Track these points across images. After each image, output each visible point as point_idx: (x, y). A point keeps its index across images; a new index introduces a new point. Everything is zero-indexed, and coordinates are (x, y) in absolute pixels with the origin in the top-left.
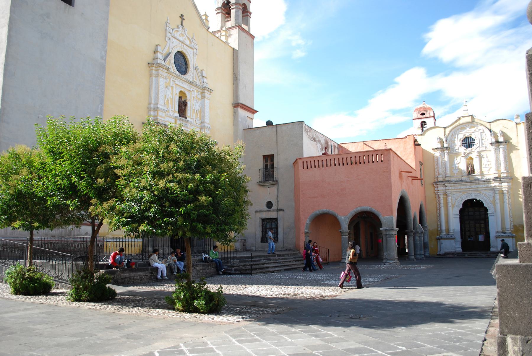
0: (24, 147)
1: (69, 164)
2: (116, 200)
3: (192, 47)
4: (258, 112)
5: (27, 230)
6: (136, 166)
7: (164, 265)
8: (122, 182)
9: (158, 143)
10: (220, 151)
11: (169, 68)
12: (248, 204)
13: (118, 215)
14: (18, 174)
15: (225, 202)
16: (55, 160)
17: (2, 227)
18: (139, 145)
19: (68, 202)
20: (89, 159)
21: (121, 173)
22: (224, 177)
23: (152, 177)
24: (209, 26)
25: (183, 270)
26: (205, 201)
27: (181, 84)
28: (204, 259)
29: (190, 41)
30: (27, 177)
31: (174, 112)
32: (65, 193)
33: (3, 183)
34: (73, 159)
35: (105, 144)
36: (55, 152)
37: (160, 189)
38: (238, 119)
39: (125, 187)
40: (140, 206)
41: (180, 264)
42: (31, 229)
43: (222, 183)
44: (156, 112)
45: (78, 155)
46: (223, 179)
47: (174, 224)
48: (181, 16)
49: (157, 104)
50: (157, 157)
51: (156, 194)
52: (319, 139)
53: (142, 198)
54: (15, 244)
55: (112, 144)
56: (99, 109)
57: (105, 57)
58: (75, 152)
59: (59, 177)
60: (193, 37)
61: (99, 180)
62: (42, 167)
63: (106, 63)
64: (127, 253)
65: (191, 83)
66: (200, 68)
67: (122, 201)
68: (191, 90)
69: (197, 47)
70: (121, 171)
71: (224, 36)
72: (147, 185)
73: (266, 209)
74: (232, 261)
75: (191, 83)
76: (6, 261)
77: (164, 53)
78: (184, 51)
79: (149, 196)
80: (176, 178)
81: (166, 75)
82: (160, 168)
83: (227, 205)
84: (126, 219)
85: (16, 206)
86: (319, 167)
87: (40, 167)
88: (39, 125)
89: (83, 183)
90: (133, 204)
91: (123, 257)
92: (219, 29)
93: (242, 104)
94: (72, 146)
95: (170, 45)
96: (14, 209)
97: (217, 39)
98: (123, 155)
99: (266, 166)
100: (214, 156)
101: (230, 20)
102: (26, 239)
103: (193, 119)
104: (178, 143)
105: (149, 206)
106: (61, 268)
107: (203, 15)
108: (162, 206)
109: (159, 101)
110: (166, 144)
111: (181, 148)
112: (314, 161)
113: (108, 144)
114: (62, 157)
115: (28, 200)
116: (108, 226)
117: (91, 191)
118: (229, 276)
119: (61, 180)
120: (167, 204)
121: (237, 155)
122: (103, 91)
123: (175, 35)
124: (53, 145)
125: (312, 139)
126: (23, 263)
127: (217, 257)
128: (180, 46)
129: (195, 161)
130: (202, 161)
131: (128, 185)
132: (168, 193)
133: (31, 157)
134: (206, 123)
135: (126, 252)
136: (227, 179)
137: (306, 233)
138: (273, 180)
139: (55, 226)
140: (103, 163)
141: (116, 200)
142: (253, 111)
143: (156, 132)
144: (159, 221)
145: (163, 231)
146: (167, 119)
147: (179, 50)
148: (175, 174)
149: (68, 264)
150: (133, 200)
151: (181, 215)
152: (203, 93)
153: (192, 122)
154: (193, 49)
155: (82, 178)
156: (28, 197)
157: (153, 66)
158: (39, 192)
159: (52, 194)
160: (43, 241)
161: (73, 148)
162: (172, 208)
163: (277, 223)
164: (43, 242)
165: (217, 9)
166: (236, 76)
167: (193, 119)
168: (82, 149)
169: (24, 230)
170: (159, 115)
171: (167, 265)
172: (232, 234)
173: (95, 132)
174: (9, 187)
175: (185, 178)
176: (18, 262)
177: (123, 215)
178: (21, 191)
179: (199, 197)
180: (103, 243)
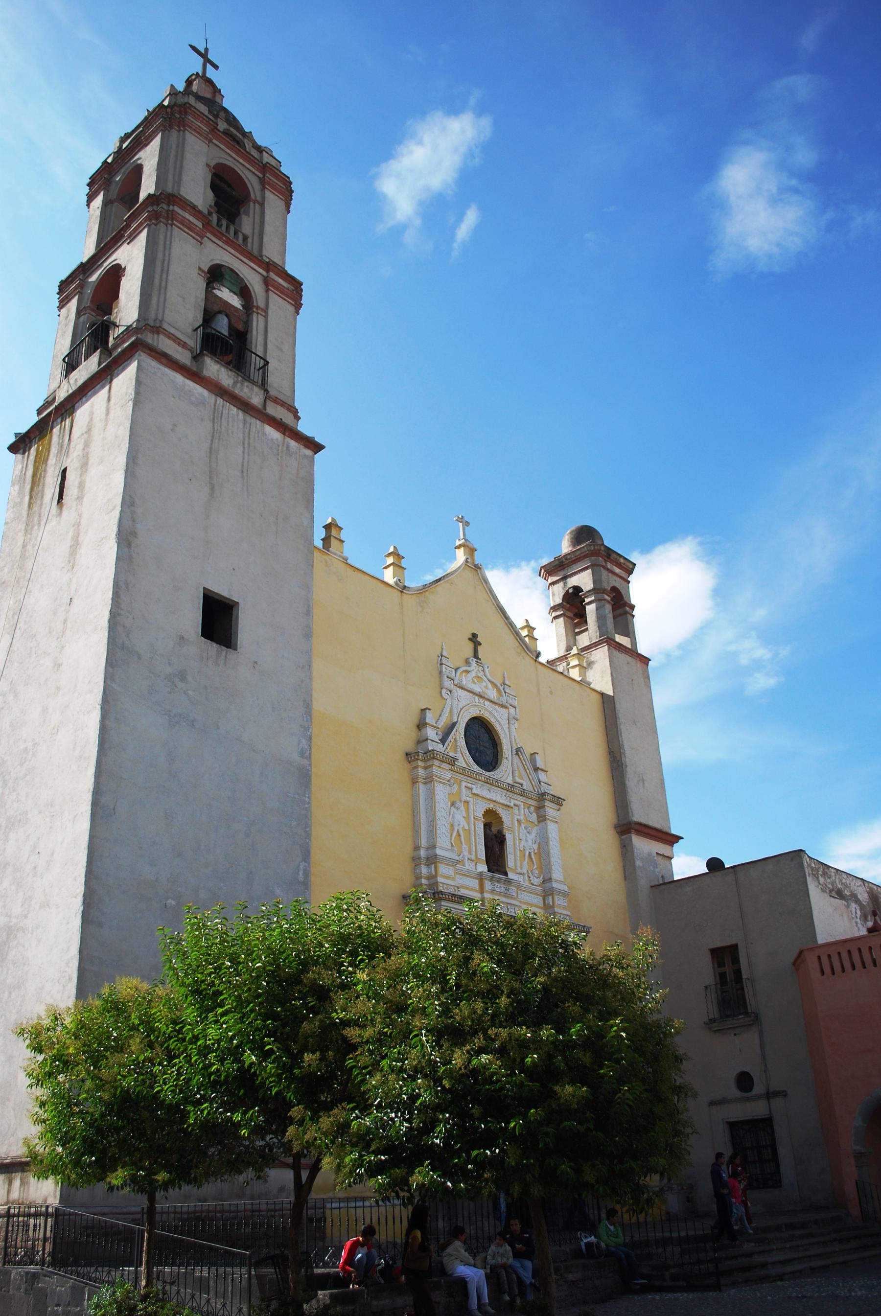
0: (135, 981)
1: (236, 1023)
2: (351, 1106)
3: (504, 702)
4: (682, 838)
5: (142, 1190)
6: (395, 1016)
7: (481, 1272)
8: (364, 1059)
9: (442, 954)
10: (598, 958)
11: (455, 759)
12: (686, 1095)
13: (357, 1146)
14: (122, 1051)
15: (623, 1095)
16: (204, 1011)
17: (85, 1185)
18: (398, 960)
19: (237, 1117)
20: (282, 1005)
21: (360, 1035)
22: (615, 1028)
23: (433, 1041)
24: (539, 649)
25: (531, 1284)
26: (573, 1096)
27: (485, 793)
28: (584, 1247)
29: (498, 690)
30: (142, 1058)
31: (476, 861)
32: (230, 1093)
33: (89, 1075)
34: (246, 1008)
35: (319, 964)
36: (204, 993)
37: (457, 1072)
38: (634, 862)
39: (370, 1073)
40: (409, 1121)
41: (522, 1266)
42: (148, 1188)
43: (612, 1046)
44: (433, 866)
45: (258, 996)
46: (612, 1034)
47: (495, 1163)
48: (471, 637)
49: (434, 847)
50: (442, 988)
51: (447, 1086)
52: (851, 892)
53: (414, 1098)
54: (113, 1225)
55: (335, 962)
56: (301, 873)
57: (308, 752)
58: (249, 989)
59: (214, 1054)
60: (504, 680)
61: (307, 1057)
62: (175, 1030)
63: (310, 765)
64: (383, 1238)
65: (510, 789)
66: (528, 750)
67: (365, 1108)
68: (512, 805)
69: (516, 703)
70: (358, 1032)
71: (577, 668)
72: (424, 1064)
73: (739, 1094)
74: (660, 1250)
75: (510, 789)
76: (93, 1269)
77: (440, 727)
78: (487, 715)
79: (430, 1094)
80: (494, 1040)
81: (448, 775)
82: (451, 1017)
83: (631, 1103)
84: (376, 1156)
85: (117, 1130)
86: (865, 967)
87: (171, 1032)
88: (166, 931)
89: (270, 1066)
90: (393, 1115)
91: (374, 1251)
92: (562, 653)
93: (640, 824)
94: (243, 977)
95: (451, 705)
96: (112, 1137)
97: (561, 676)
98: (362, 990)
99: (722, 977)
100: (583, 973)
101: (587, 630)
102: (138, 1209)
103: (523, 874)
104: (492, 947)
105: (431, 1117)
106: (221, 1289)
107: (522, 628)
108: (463, 1115)
109: (439, 840)
110: (461, 955)
111: (499, 963)
112: (849, 952)
113: (324, 964)
114: (221, 1005)
115: (146, 1114)
116: (333, 1176)
117: (289, 1087)
118: (657, 1297)
119: (218, 1061)
120: (476, 1111)
121: (643, 966)
122: (307, 829)
123: (461, 681)
124: (199, 976)
125: (834, 894)
126: (132, 1276)
127: (620, 1240)
128: (477, 704)
129: (539, 991)
130: (554, 990)
131: (376, 1065)
132: (476, 1079)
133: (150, 1008)
134: (556, 881)
135: (382, 1236)
136: (624, 1034)
137: (858, 1156)
138: (746, 1013)
139: (207, 1175)
140: (316, 1014)
141: (351, 1106)
142: (670, 838)
143: (437, 925)
144: (459, 1157)
145: (471, 1185)
146: (460, 880)
147: (474, 713)
148: (490, 1032)
149: (240, 1273)
150: (394, 1104)
151: (512, 1137)
152: (540, 808)
153: (522, 882)
154: (506, 707)
155: (265, 1055)
156: (143, 1107)
157: (417, 759)
158: (167, 1091)
159: (198, 1096)
160: (178, 1213)
161: (246, 981)
162: (490, 1122)
163: (773, 1131)
164: (179, 1216)
165: (552, 608)
166: (615, 757)
167: (523, 874)
168: (264, 980)
169: (133, 1190)
170: (440, 873)
171: (488, 1271)
172: (654, 1181)
173: (296, 937)
174: (101, 1084)
175: (517, 1040)
176: (119, 1273)
177: (368, 1145)
178: (128, 1091)
179: (557, 1088)
180: (324, 1213)
